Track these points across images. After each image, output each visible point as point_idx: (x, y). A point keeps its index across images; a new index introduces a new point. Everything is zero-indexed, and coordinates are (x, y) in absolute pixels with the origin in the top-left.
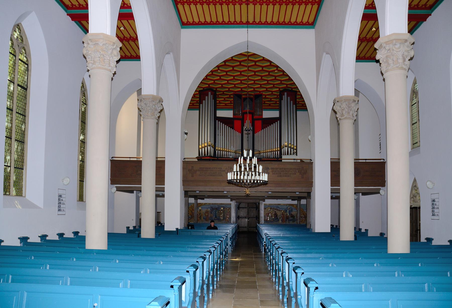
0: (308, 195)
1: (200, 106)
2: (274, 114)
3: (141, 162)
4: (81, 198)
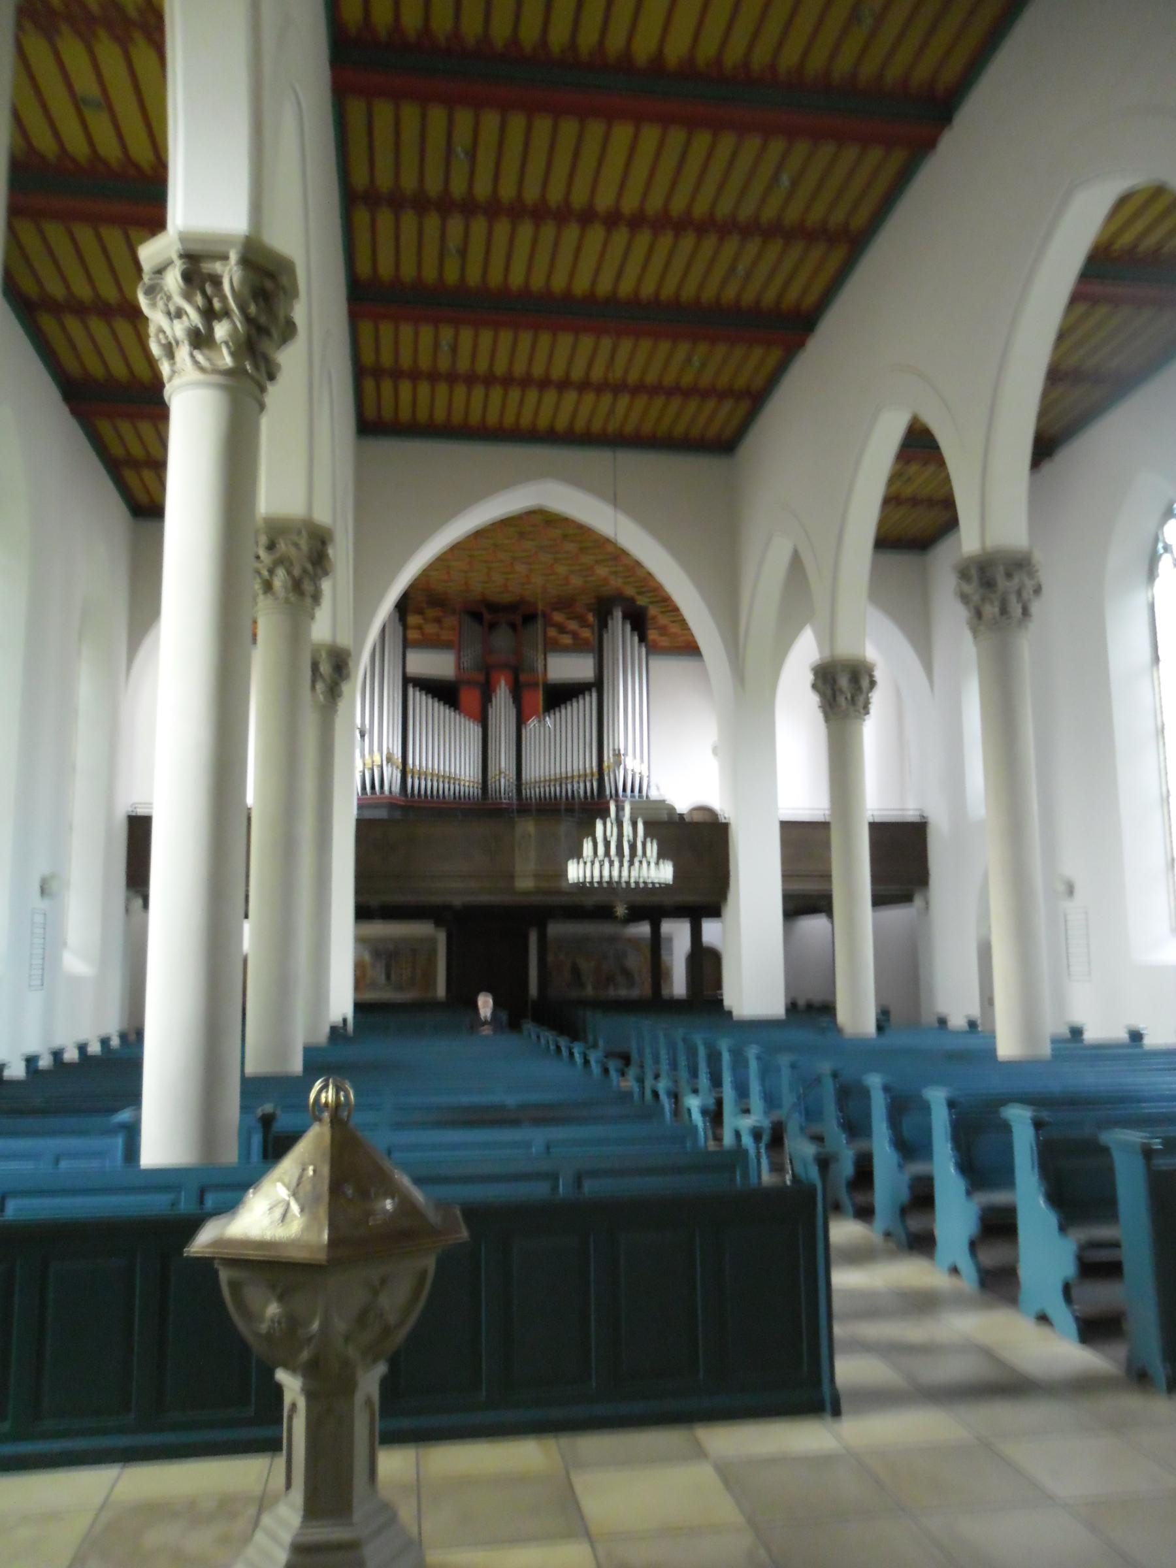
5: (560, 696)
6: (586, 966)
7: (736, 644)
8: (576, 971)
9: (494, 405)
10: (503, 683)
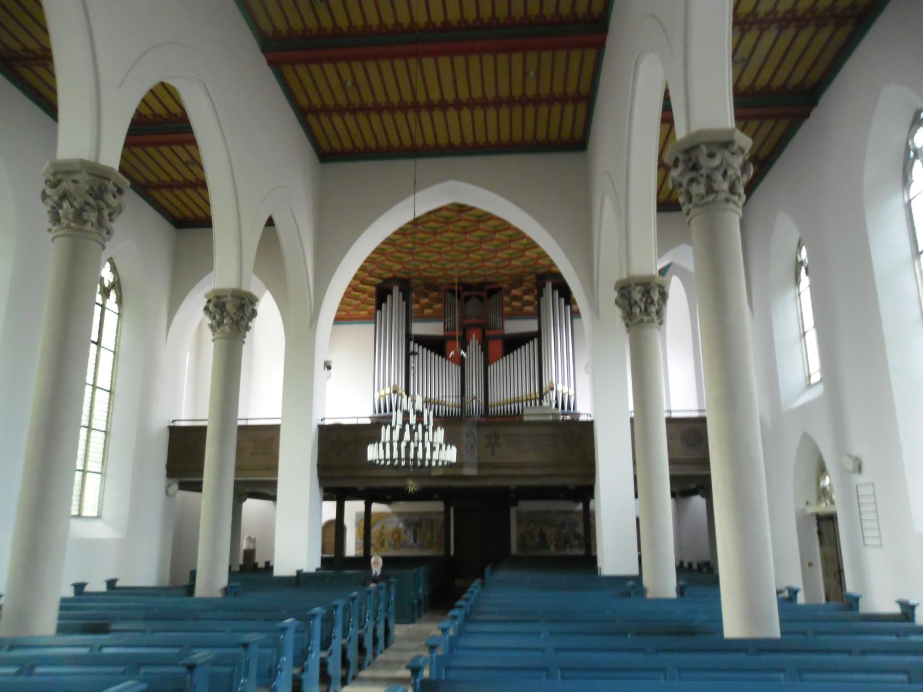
0: (586, 492)
1: (376, 314)
2: (530, 326)
3: (589, 427)
4: (638, 520)
5: (513, 343)
6: (550, 532)
7: (592, 285)
8: (543, 536)
9: (398, 128)
10: (474, 336)
